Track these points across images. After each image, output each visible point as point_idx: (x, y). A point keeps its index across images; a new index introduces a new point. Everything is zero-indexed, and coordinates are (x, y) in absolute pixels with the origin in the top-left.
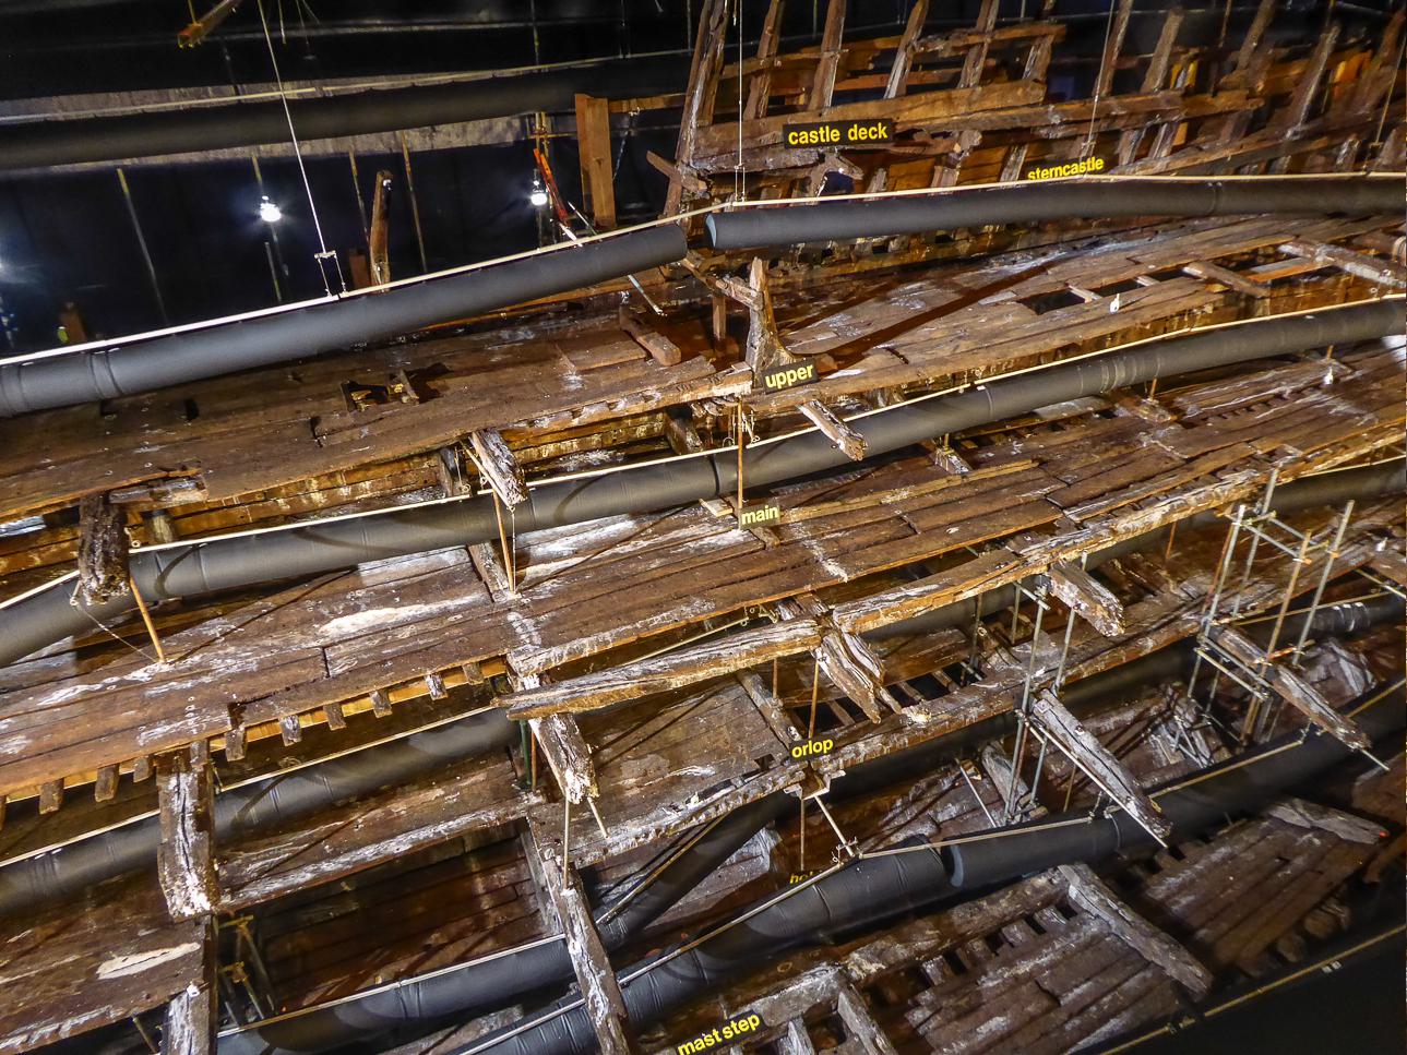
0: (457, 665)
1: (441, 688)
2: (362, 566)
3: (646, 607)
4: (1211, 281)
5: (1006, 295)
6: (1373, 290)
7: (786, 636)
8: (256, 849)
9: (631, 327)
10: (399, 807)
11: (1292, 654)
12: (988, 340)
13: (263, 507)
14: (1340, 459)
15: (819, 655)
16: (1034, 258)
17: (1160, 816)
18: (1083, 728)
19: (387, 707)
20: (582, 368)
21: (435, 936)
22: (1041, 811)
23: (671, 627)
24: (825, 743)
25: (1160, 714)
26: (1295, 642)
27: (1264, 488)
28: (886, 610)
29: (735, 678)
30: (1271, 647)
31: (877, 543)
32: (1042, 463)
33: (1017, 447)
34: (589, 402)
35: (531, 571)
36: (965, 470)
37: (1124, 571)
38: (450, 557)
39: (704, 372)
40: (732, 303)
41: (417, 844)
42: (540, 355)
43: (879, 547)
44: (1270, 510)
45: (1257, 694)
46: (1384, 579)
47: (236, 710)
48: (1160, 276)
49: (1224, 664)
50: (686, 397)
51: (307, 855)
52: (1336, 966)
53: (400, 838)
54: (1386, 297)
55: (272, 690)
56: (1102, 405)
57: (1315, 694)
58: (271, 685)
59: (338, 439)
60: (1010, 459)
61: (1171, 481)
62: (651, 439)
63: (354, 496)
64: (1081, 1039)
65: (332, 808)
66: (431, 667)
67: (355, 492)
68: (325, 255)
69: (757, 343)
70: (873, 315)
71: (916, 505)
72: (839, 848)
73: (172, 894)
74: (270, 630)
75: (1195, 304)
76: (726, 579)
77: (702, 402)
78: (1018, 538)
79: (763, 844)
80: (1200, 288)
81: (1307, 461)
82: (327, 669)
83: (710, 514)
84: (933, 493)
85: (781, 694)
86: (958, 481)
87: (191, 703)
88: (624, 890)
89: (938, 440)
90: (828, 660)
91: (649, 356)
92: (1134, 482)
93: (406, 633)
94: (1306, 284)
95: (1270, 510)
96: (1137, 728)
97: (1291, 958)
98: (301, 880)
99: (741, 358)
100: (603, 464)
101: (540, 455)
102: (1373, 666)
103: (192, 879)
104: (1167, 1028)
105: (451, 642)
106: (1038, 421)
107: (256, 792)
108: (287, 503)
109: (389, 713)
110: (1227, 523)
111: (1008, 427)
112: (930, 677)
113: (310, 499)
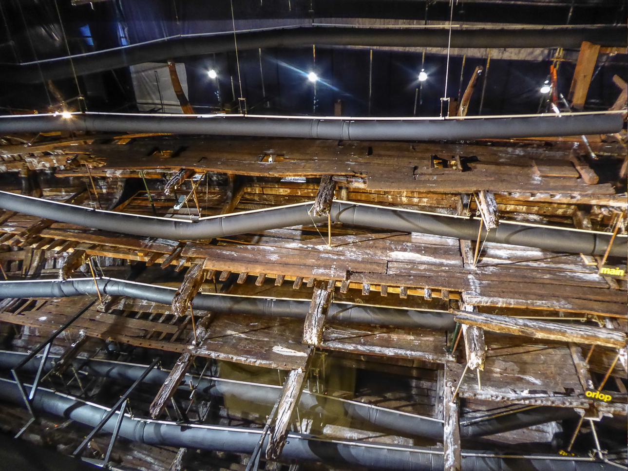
0: (440, 288)
1: (430, 295)
3: (535, 295)
9: (575, 161)
10: (394, 337)
20: (544, 174)
23: (545, 309)
24: (607, 396)
29: (567, 345)
34: (542, 191)
38: (451, 242)
39: (608, 192)
41: (397, 355)
47: (349, 274)
58: (364, 269)
59: (423, 178)
62: (564, 216)
63: (419, 203)
66: (429, 285)
67: (420, 201)
68: (445, 99)
77: (601, 207)
82: (387, 270)
83: (584, 262)
85: (590, 362)
91: (580, 177)
93: (423, 267)
98: (349, 348)
100: (535, 222)
101: (506, 209)
103: (315, 331)
107: (344, 308)
109: (406, 297)
113: (401, 199)
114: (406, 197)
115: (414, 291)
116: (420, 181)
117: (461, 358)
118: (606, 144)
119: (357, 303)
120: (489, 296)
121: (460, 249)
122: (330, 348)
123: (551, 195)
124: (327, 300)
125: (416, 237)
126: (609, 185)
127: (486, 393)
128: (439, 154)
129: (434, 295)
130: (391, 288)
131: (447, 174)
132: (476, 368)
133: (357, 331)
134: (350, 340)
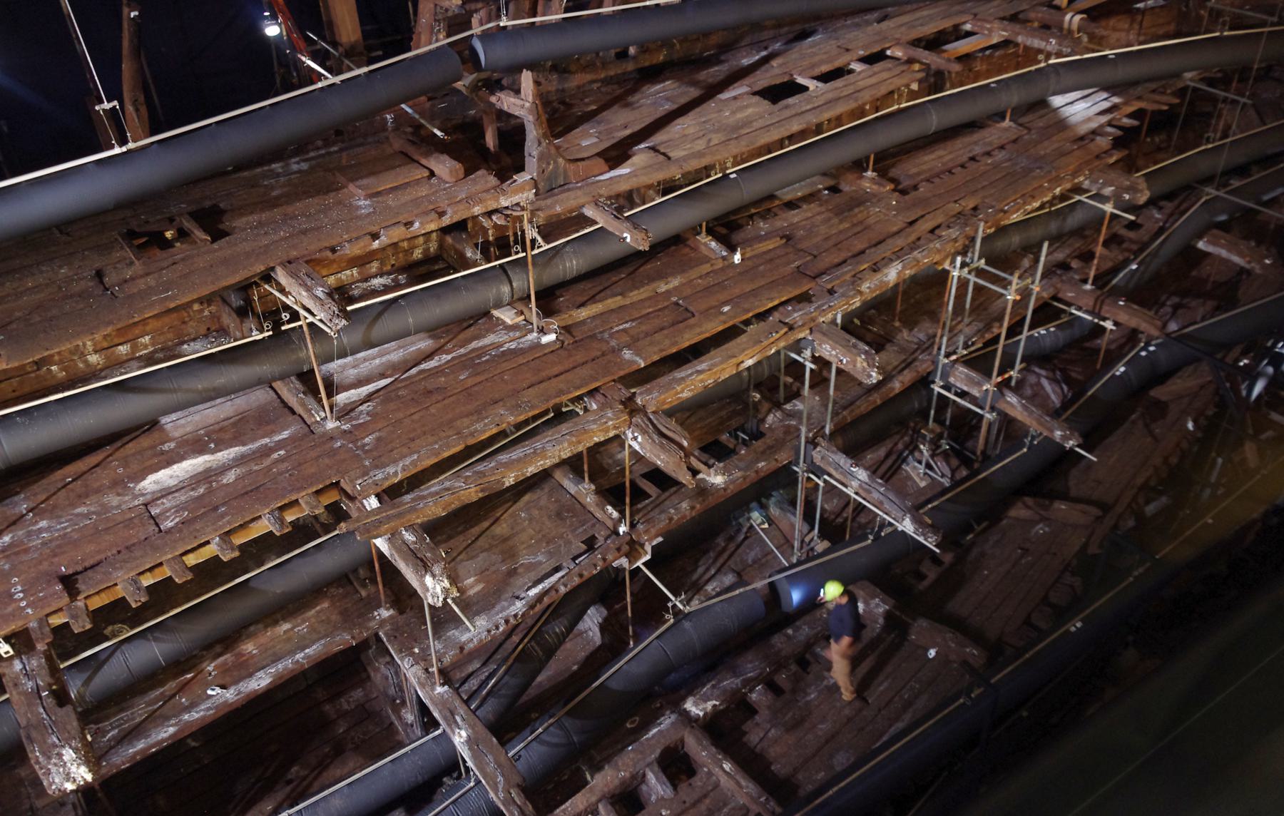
0: (294, 498)
1: (281, 521)
2: (165, 420)
3: (467, 416)
4: (910, 61)
5: (740, 89)
6: (1041, 57)
7: (598, 423)
8: (107, 718)
9: (411, 150)
10: (249, 647)
11: (1010, 378)
12: (734, 131)
13: (37, 377)
14: (1029, 208)
15: (630, 436)
16: (758, 52)
17: (932, 526)
18: (857, 465)
19: (233, 549)
20: (370, 192)
21: (295, 769)
22: (826, 544)
25: (906, 447)
26: (1012, 368)
27: (973, 240)
28: (692, 382)
29: (545, 475)
30: (995, 373)
31: (662, 329)
32: (788, 238)
33: (763, 226)
35: (342, 398)
36: (724, 253)
37: (867, 326)
38: (260, 396)
39: (489, 185)
40: (502, 115)
41: (278, 676)
42: (322, 183)
43: (665, 332)
44: (980, 258)
45: (988, 416)
46: (1069, 305)
47: (69, 583)
48: (870, 60)
49: (956, 394)
50: (477, 210)
51: (165, 710)
52: (1079, 625)
53: (259, 674)
54: (1051, 62)
55: (102, 556)
56: (831, 182)
57: (1023, 409)
58: (99, 552)
59: (133, 289)
60: (760, 239)
61: (900, 242)
62: (428, 260)
63: (133, 353)
64: (890, 726)
65: (181, 665)
66: (267, 506)
67: (135, 348)
69: (535, 153)
70: (622, 122)
71: (688, 291)
72: (670, 605)
73: (48, 773)
74: (82, 497)
75: (897, 80)
76: (534, 379)
77: (489, 214)
78: (781, 309)
79: (592, 621)
80: (905, 68)
81: (1005, 212)
82: (157, 525)
83: (504, 322)
84: (700, 277)
85: (592, 480)
86: (720, 264)
87: (15, 585)
88: (495, 676)
89: (695, 230)
90: (640, 439)
91: (432, 174)
92: (870, 247)
93: (230, 477)
94: (982, 59)
95: (980, 258)
96: (890, 462)
97: (1043, 625)
98: (165, 735)
99: (521, 168)
100: (387, 289)
102: (1068, 380)
103: (68, 754)
104: (962, 701)
105: (281, 478)
106: (777, 202)
107: (96, 663)
108: (61, 370)
109: (237, 554)
110: (946, 273)
111: (753, 211)
112: (717, 443)
113: (86, 362)
114: (96, 352)
115: (243, 533)
116: (131, 297)
117: (404, 597)
118: (436, 102)
119: (115, 636)
120: (395, 461)
121: (283, 401)
122: (118, 766)
123: (406, 224)
124: (54, 670)
125: (177, 424)
126: (481, 172)
127: (475, 631)
128: (134, 225)
129: (290, 517)
130: (96, 598)
131: (183, 259)
132: (445, 599)
133: (158, 692)
134: (154, 719)
